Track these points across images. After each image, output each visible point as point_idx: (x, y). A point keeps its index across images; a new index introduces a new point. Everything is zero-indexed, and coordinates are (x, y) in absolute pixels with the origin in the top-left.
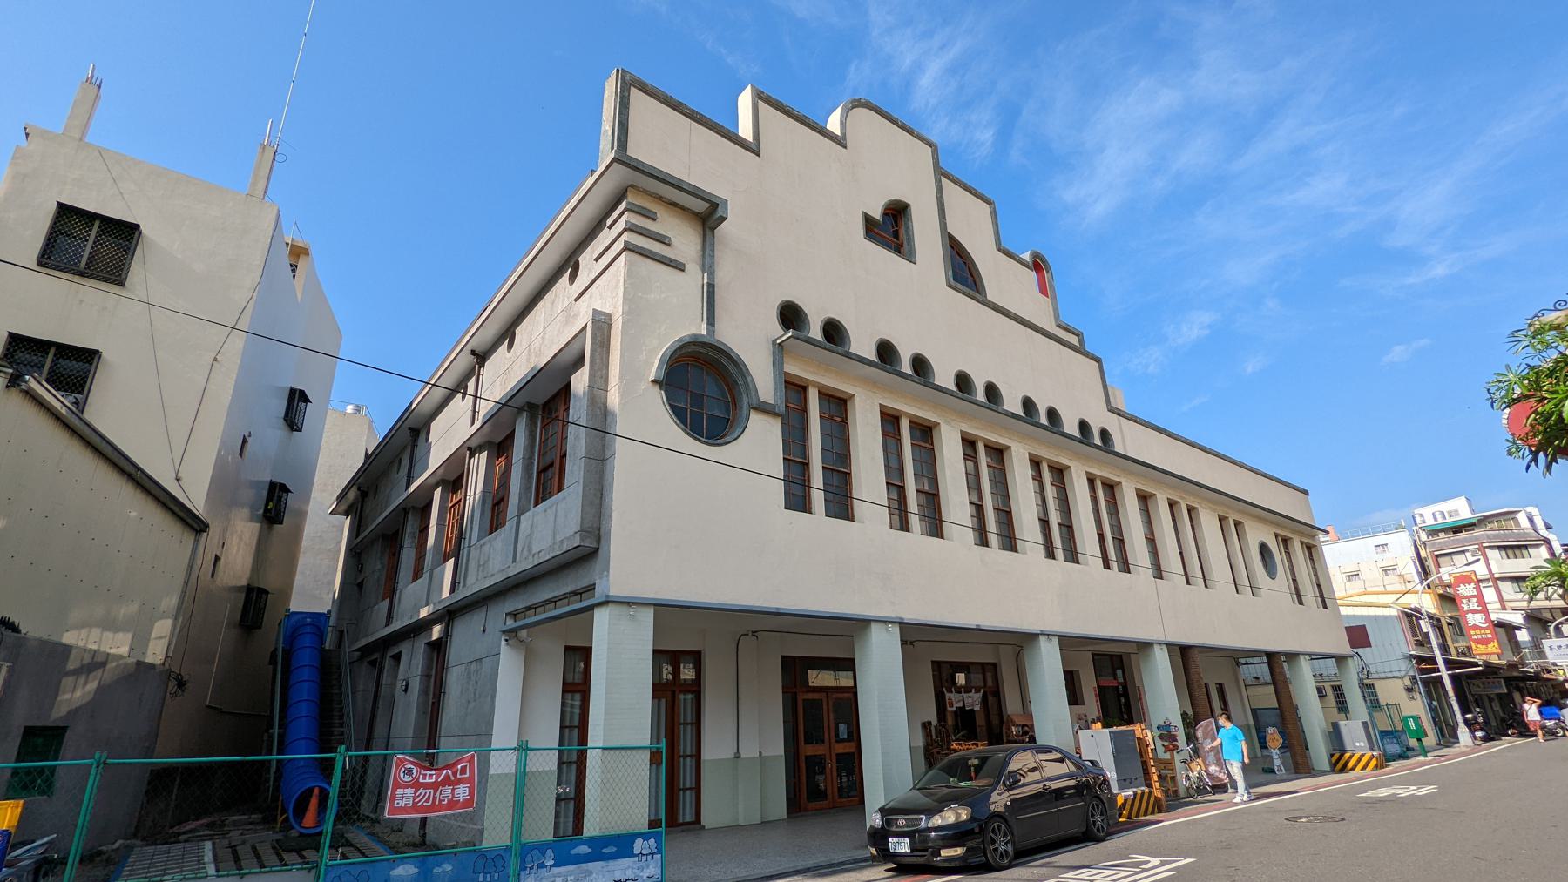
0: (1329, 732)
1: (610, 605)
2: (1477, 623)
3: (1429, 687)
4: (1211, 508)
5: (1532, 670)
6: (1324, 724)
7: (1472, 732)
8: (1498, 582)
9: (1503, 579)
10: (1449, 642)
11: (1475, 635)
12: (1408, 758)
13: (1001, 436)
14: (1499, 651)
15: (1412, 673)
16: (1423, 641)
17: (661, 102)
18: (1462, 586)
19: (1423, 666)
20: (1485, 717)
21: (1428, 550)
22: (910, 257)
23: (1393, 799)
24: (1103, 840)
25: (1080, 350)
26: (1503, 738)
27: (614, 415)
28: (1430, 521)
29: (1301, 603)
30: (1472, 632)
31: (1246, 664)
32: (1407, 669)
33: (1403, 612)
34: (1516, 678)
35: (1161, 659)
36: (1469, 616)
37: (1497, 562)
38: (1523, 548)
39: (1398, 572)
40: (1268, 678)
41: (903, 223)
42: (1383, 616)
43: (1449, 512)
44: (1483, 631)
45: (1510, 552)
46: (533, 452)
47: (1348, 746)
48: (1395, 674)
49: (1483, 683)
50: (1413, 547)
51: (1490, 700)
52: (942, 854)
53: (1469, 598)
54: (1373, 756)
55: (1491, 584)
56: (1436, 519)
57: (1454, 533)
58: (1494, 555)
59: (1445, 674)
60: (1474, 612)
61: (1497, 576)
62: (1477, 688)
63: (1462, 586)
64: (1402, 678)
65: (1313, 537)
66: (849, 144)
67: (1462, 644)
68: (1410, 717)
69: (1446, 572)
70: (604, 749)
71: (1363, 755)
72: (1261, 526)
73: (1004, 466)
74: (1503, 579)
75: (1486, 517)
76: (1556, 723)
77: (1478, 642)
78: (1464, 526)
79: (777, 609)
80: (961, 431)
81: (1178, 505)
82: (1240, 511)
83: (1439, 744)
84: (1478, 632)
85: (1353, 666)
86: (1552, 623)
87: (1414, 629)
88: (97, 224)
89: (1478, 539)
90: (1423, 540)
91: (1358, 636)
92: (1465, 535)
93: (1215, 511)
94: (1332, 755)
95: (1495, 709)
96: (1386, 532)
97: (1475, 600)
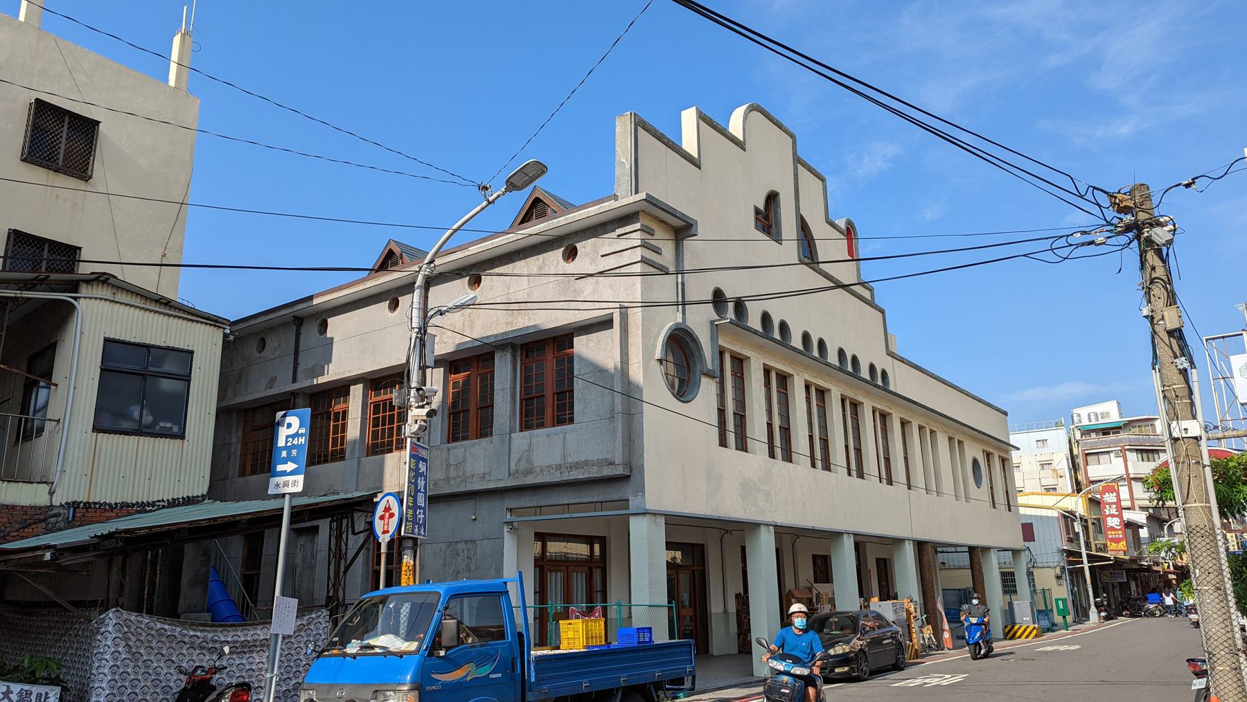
0: (1005, 611)
1: (647, 516)
2: (1114, 525)
3: (1073, 576)
4: (945, 431)
5: (1146, 564)
6: (1002, 603)
7: (1099, 612)
8: (1132, 481)
9: (1136, 479)
10: (1092, 540)
11: (1111, 534)
12: (1054, 631)
13: (825, 382)
14: (1126, 548)
15: (1062, 564)
16: (1074, 538)
17: (652, 135)
18: (1107, 494)
19: (1071, 559)
20: (1108, 599)
21: (1080, 448)
22: (779, 240)
23: (1057, 651)
24: (903, 670)
25: (871, 304)
26: (1119, 618)
27: (639, 389)
28: (1085, 422)
29: (994, 507)
30: (1109, 533)
31: (943, 552)
32: (1058, 560)
33: (1061, 514)
34: (1135, 570)
35: (909, 551)
36: (1109, 519)
37: (1133, 463)
38: (1155, 452)
39: (1053, 467)
40: (967, 562)
41: (773, 207)
42: (1047, 516)
43: (1102, 414)
44: (1117, 532)
45: (1145, 455)
46: (515, 383)
47: (1018, 620)
48: (1050, 565)
49: (1111, 574)
50: (1068, 445)
51: (1114, 587)
52: (836, 671)
53: (1110, 504)
54: (1035, 628)
55: (1126, 483)
56: (1090, 421)
57: (1104, 434)
58: (1132, 457)
59: (1086, 566)
60: (1113, 516)
61: (1132, 476)
62: (1106, 578)
63: (1107, 494)
64: (1055, 567)
65: (1007, 452)
66: (747, 147)
67: (1101, 541)
68: (1060, 600)
69: (1096, 470)
70: (650, 606)
71: (1028, 627)
72: (975, 444)
73: (824, 404)
74: (1136, 479)
75: (1130, 422)
76: (1156, 607)
77: (1113, 540)
78: (1112, 428)
79: (719, 517)
80: (805, 380)
81: (924, 429)
82: (964, 433)
83: (1074, 622)
84: (1113, 533)
85: (1024, 557)
86: (1167, 522)
87: (1069, 528)
88: (67, 119)
89: (1121, 442)
90: (1078, 439)
91: (1028, 531)
92: (1112, 437)
93: (946, 432)
94: (1006, 627)
95: (1116, 595)
96: (1047, 427)
97: (1115, 506)
